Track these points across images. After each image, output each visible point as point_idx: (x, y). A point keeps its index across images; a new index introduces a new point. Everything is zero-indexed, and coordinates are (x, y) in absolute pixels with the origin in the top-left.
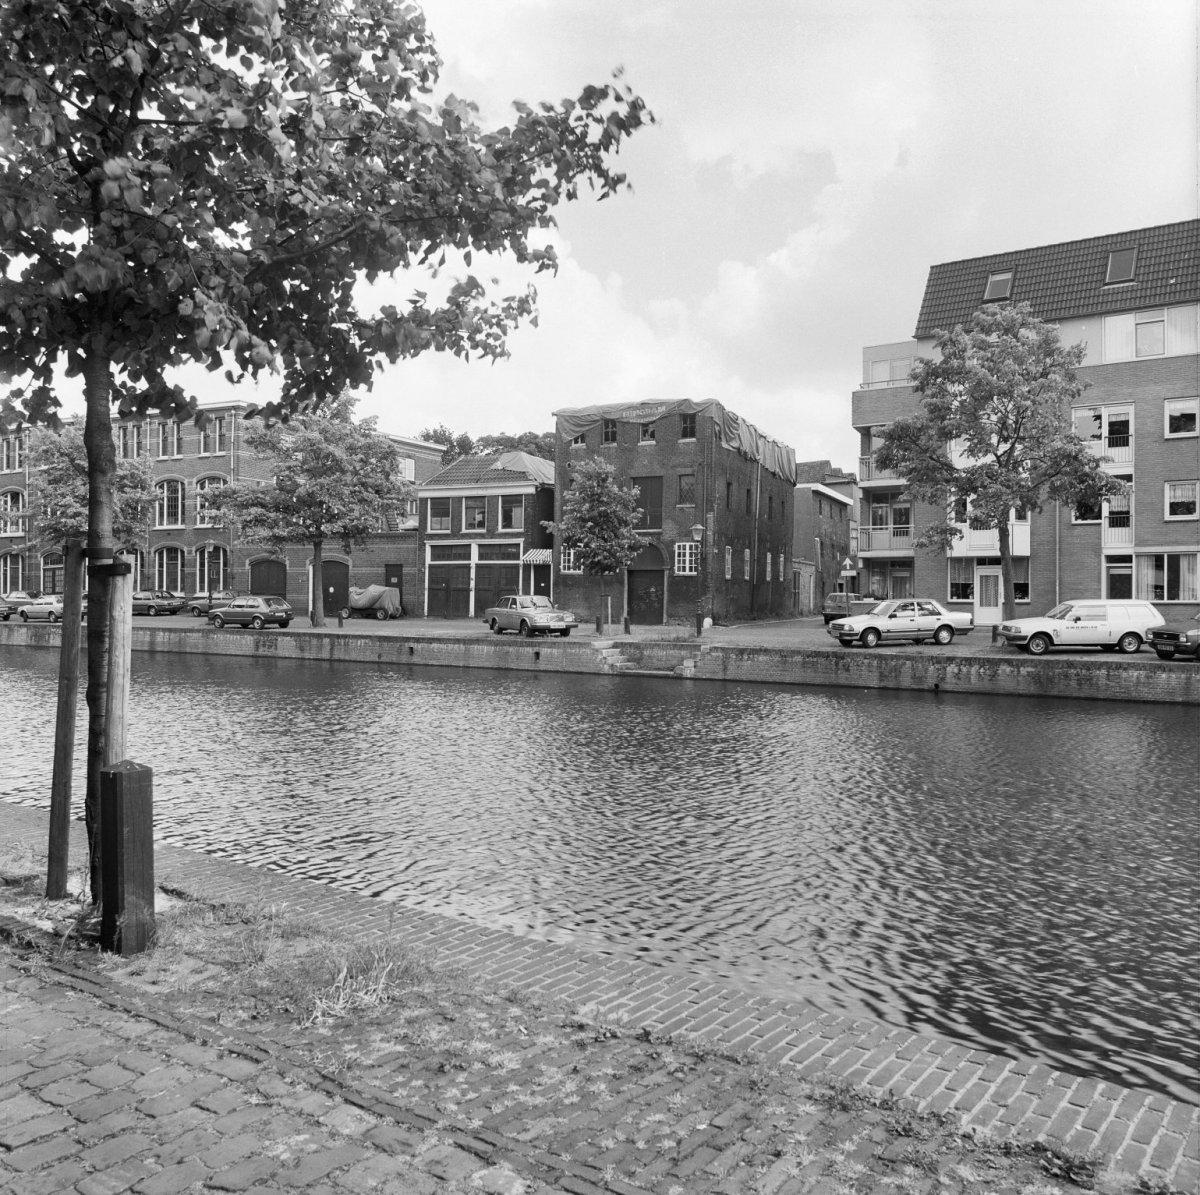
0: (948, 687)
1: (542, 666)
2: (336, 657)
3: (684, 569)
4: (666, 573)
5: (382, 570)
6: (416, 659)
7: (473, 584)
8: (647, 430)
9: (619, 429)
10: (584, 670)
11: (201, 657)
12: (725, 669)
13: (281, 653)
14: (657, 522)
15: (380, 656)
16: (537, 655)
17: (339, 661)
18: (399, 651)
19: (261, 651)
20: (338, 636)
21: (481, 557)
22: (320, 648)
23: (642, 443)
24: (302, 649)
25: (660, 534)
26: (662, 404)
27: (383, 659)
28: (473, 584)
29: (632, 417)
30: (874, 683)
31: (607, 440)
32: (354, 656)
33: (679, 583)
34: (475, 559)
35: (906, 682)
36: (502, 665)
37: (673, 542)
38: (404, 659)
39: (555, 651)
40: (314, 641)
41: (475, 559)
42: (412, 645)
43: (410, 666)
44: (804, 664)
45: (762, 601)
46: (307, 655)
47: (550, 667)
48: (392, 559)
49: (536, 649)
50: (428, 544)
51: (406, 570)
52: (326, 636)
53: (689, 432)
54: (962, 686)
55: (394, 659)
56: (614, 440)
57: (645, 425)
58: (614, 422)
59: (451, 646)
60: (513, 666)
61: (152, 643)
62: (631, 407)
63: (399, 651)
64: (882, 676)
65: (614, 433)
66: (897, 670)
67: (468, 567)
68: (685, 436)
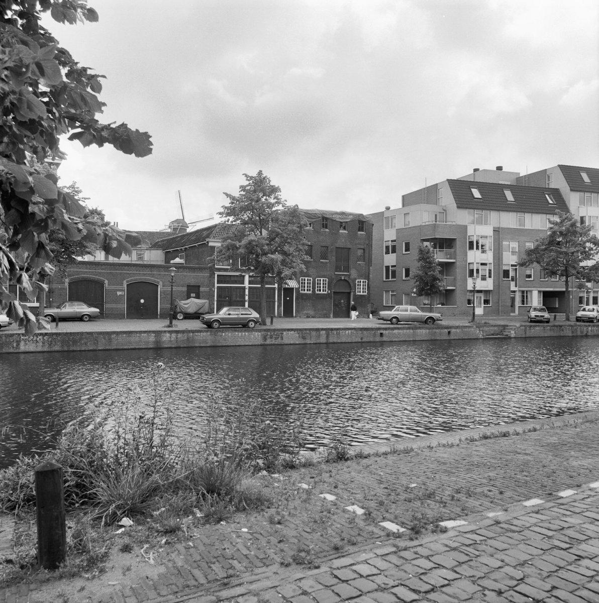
0: (589, 334)
1: (452, 337)
2: (331, 340)
3: (320, 291)
4: (352, 293)
5: (185, 289)
6: (385, 339)
7: (247, 298)
8: (343, 225)
9: (329, 224)
10: (471, 337)
11: (325, 345)
12: (526, 333)
13: (286, 341)
14: (347, 269)
15: (362, 339)
16: (449, 332)
17: (334, 343)
18: (375, 335)
19: (268, 342)
20: (332, 329)
21: (250, 283)
22: (319, 336)
23: (341, 231)
24: (304, 338)
25: (349, 275)
26: (351, 214)
27: (363, 340)
28: (247, 298)
29: (338, 218)
30: (571, 335)
31: (323, 227)
32: (344, 340)
33: (359, 298)
34: (247, 284)
35: (579, 333)
36: (433, 338)
37: (356, 279)
38: (378, 339)
39: (458, 330)
40: (314, 333)
41: (247, 284)
42: (382, 331)
43: (449, 341)
44: (550, 330)
45: (342, 301)
46: (308, 341)
47: (455, 338)
48: (193, 282)
49: (449, 330)
50: (217, 273)
51: (202, 289)
52: (323, 329)
53: (361, 229)
54: (593, 334)
55: (372, 340)
56: (326, 228)
57: (341, 223)
58: (327, 219)
59: (405, 331)
60: (438, 338)
61: (157, 342)
62: (337, 213)
63: (375, 335)
64: (573, 332)
65: (326, 224)
66: (576, 330)
67: (244, 288)
68: (359, 230)
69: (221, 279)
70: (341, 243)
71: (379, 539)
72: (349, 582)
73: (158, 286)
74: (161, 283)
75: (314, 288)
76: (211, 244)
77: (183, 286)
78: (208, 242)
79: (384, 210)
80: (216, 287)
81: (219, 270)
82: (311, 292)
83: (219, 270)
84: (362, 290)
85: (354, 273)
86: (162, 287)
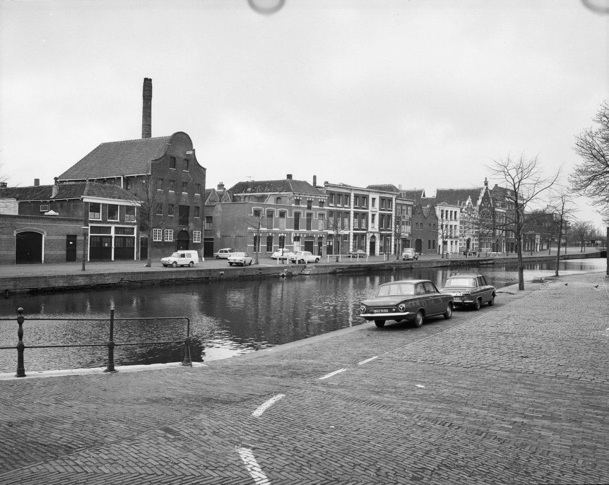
5: (65, 238)
34: (113, 234)
48: (71, 232)
51: (78, 238)
69: (94, 229)
70: (184, 202)
71: (113, 433)
72: (191, 474)
73: (42, 235)
74: (45, 233)
75: (163, 238)
76: (85, 200)
77: (563, 276)
78: (82, 199)
79: (285, 178)
80: (89, 236)
81: (92, 222)
82: (161, 240)
83: (92, 222)
84: (169, 238)
85: (191, 225)
86: (46, 236)
